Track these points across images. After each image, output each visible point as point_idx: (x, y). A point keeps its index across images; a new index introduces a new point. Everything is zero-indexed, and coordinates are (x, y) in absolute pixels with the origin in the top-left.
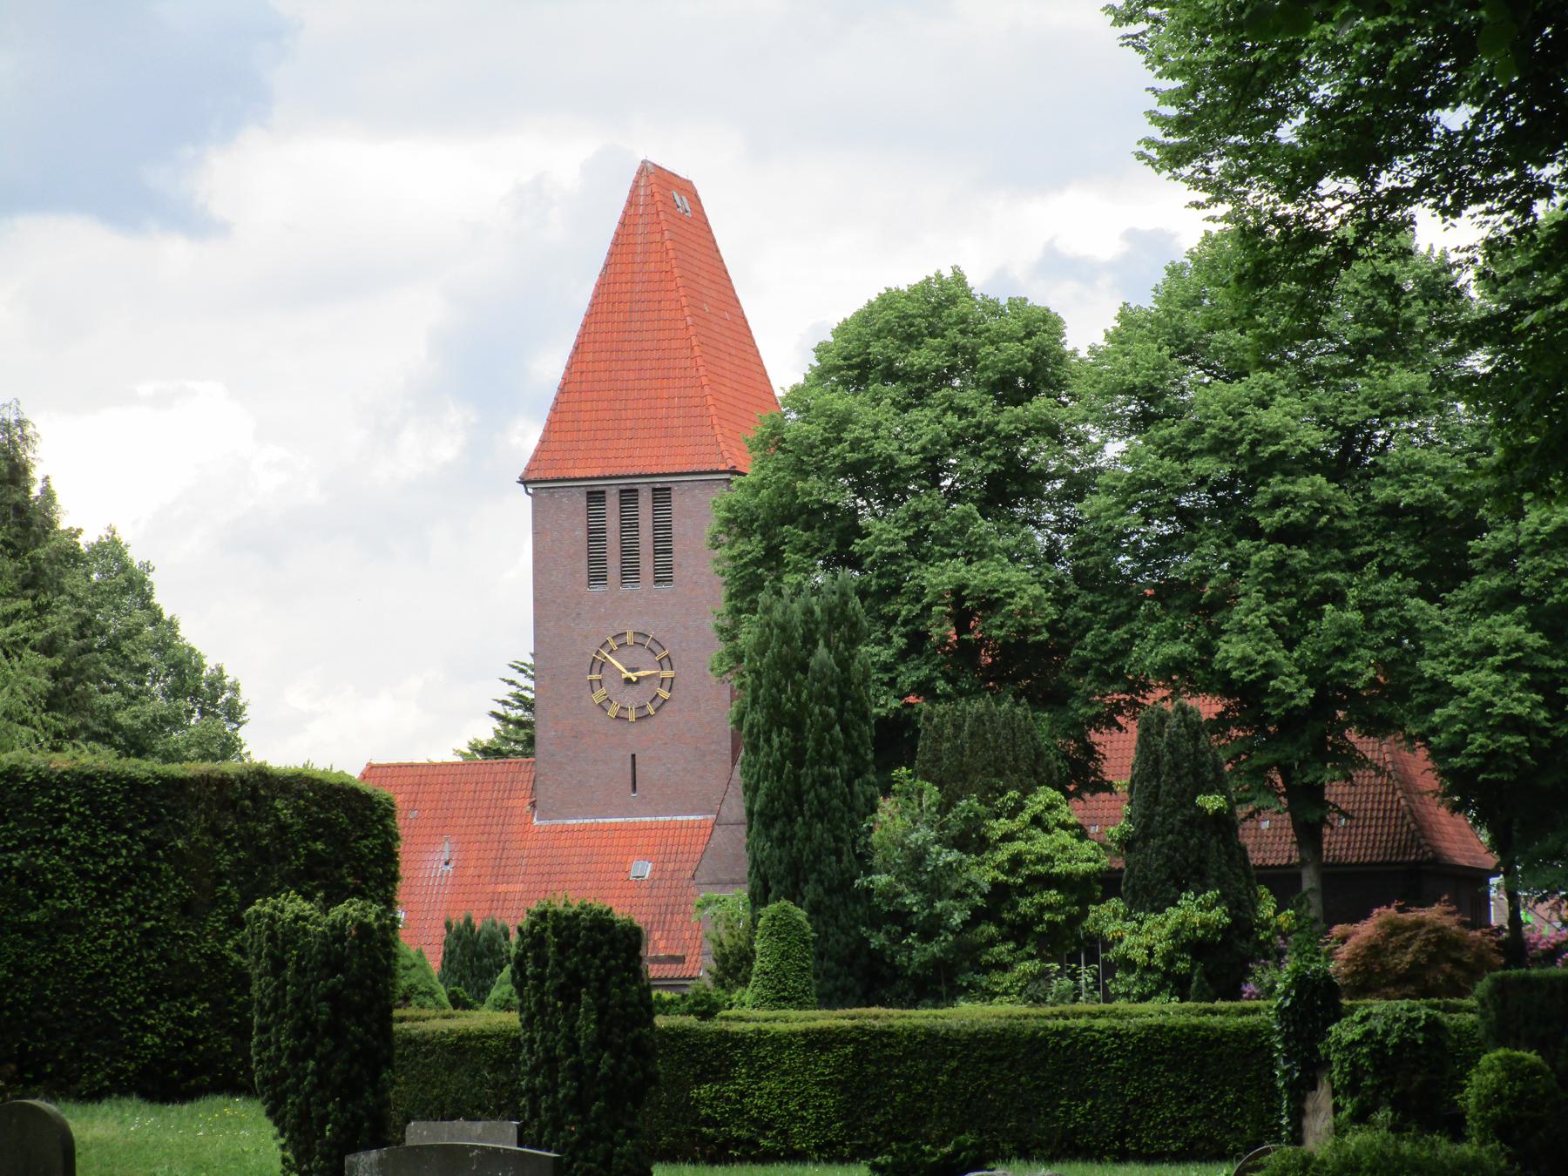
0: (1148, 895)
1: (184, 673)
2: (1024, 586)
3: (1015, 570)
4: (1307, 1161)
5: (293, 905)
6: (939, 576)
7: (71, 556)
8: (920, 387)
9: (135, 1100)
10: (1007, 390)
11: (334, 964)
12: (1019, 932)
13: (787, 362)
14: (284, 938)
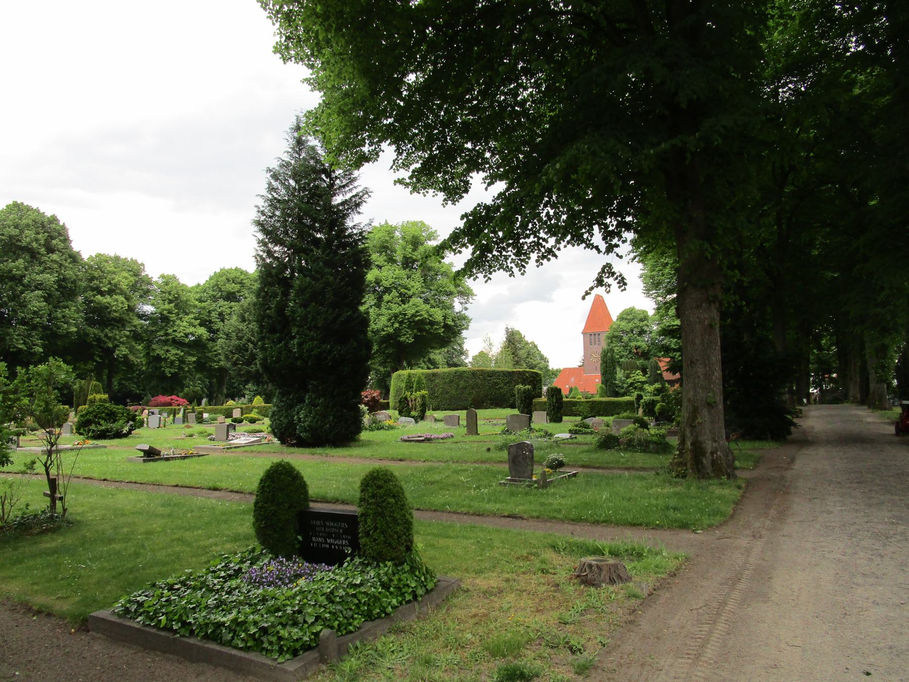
0: (651, 383)
1: (543, 358)
2: (644, 345)
3: (643, 343)
4: (286, 434)
5: (520, 386)
6: (633, 344)
7: (527, 343)
8: (629, 321)
9: (866, 407)
10: (641, 320)
11: (524, 393)
12: (635, 388)
13: (614, 318)
14: (519, 390)
